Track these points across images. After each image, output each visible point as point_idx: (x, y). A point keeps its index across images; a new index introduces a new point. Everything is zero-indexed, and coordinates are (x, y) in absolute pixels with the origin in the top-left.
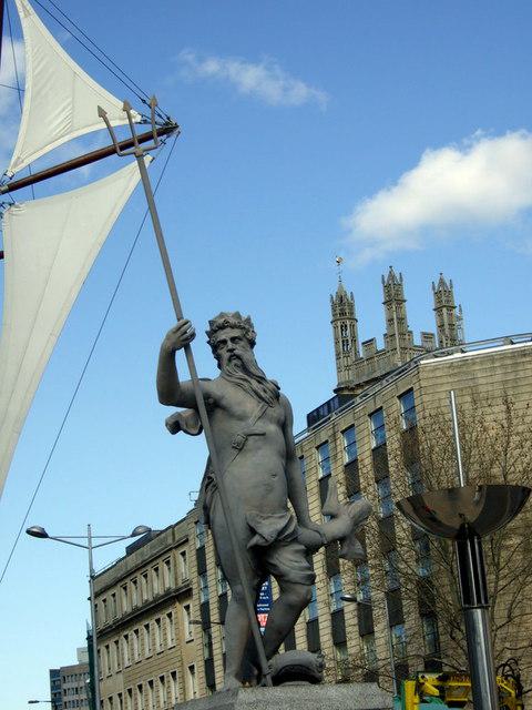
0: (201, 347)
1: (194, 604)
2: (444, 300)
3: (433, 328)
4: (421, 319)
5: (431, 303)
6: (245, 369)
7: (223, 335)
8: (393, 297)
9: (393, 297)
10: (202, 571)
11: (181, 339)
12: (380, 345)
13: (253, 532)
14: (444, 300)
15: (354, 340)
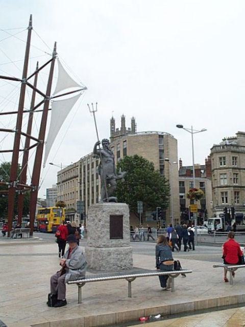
0: (101, 146)
1: (79, 178)
2: (133, 121)
3: (130, 127)
4: (128, 125)
5: (130, 122)
6: (107, 148)
7: (104, 143)
8: (123, 120)
9: (123, 120)
10: (81, 173)
11: (98, 144)
12: (120, 130)
13: (107, 177)
14: (133, 121)
15: (114, 128)
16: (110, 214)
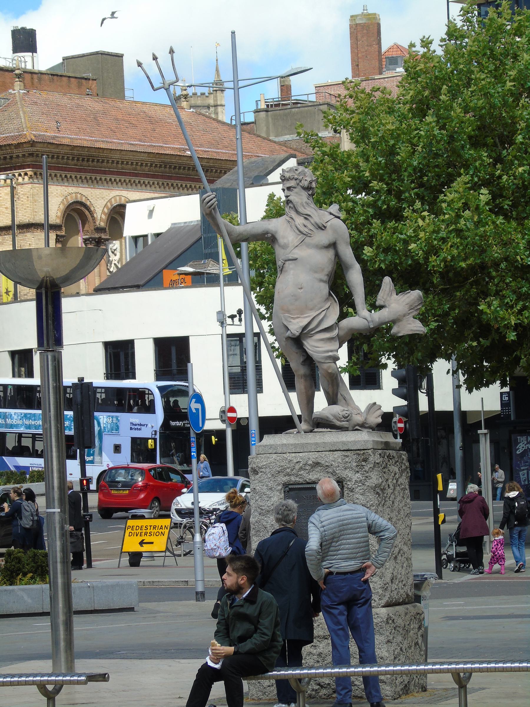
16: (285, 479)
